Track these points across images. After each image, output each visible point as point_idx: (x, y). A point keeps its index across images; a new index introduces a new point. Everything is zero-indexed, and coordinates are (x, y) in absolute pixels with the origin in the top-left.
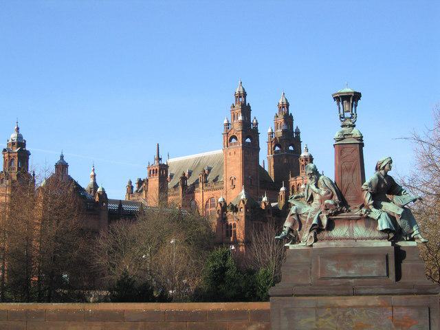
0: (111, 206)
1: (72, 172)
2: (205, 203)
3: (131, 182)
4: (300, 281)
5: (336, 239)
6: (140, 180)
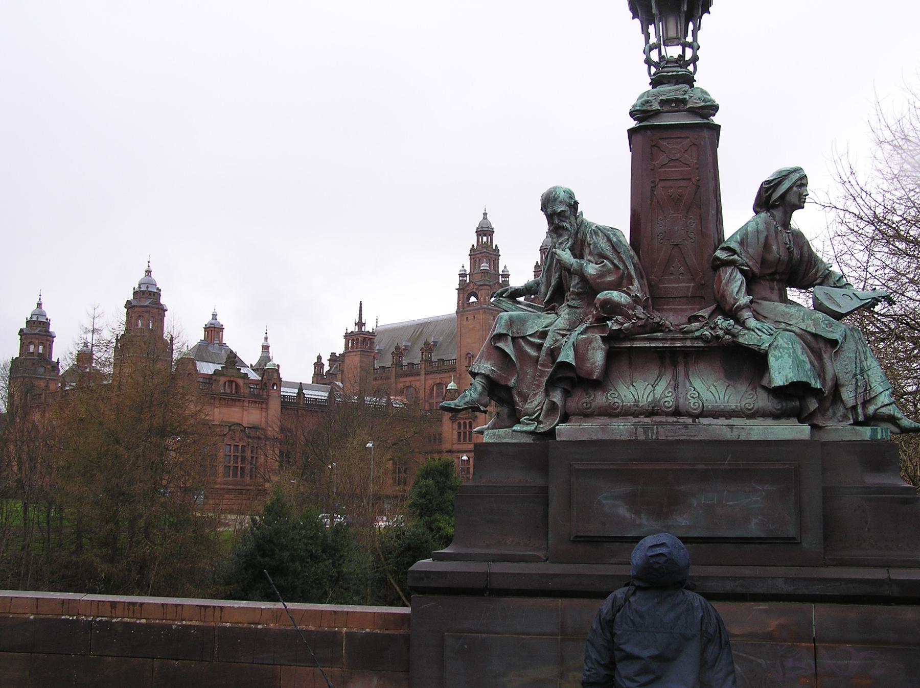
0: (285, 391)
1: (230, 339)
2: (428, 391)
3: (319, 358)
4: (808, 366)
5: (626, 413)
6: (333, 354)
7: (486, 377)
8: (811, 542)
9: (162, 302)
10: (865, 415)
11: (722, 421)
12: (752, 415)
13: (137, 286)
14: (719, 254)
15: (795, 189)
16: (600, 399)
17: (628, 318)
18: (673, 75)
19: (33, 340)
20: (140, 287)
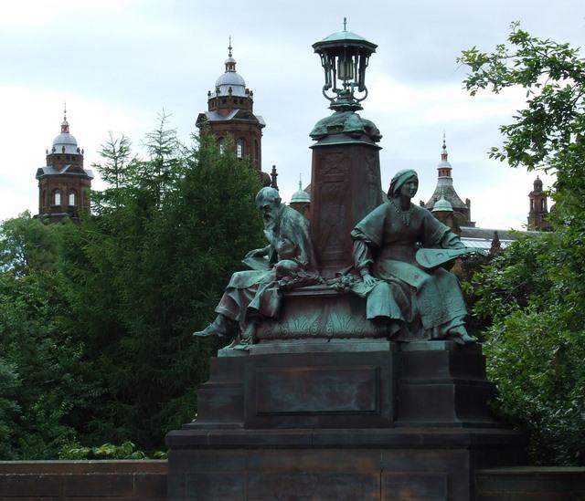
7: (223, 315)
8: (388, 413)
9: (256, 112)
10: (439, 333)
11: (345, 341)
12: (362, 336)
13: (213, 90)
14: (353, 233)
15: (405, 186)
16: (277, 328)
17: (292, 277)
18: (346, 105)
19: (60, 186)
20: (218, 91)
